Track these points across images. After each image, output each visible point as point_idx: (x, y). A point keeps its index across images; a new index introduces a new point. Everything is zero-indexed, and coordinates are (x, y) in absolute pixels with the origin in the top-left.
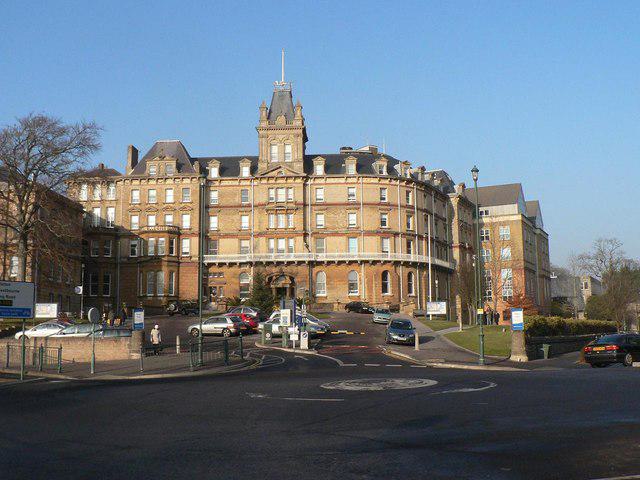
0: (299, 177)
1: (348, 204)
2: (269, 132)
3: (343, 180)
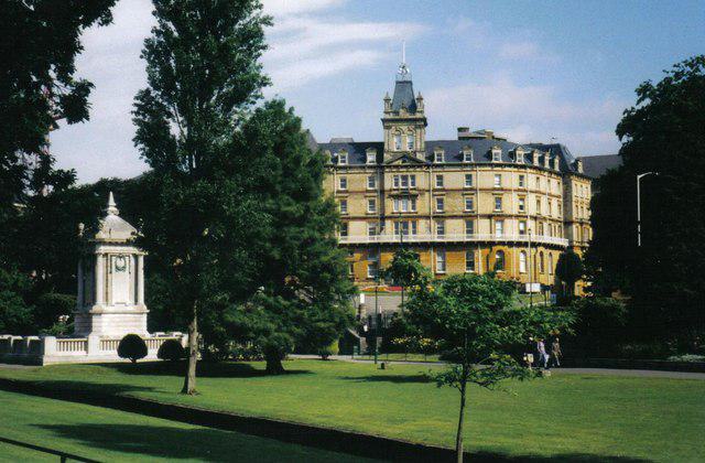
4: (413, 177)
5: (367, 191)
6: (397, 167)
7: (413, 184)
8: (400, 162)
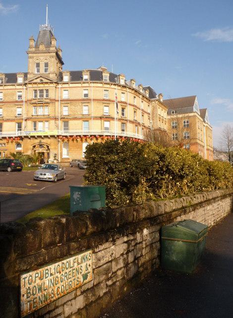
0: (52, 83)
1: (84, 100)
2: (35, 55)
3: (79, 85)
4: (47, 91)
5: (17, 102)
6: (36, 83)
7: (47, 96)
8: (38, 81)
